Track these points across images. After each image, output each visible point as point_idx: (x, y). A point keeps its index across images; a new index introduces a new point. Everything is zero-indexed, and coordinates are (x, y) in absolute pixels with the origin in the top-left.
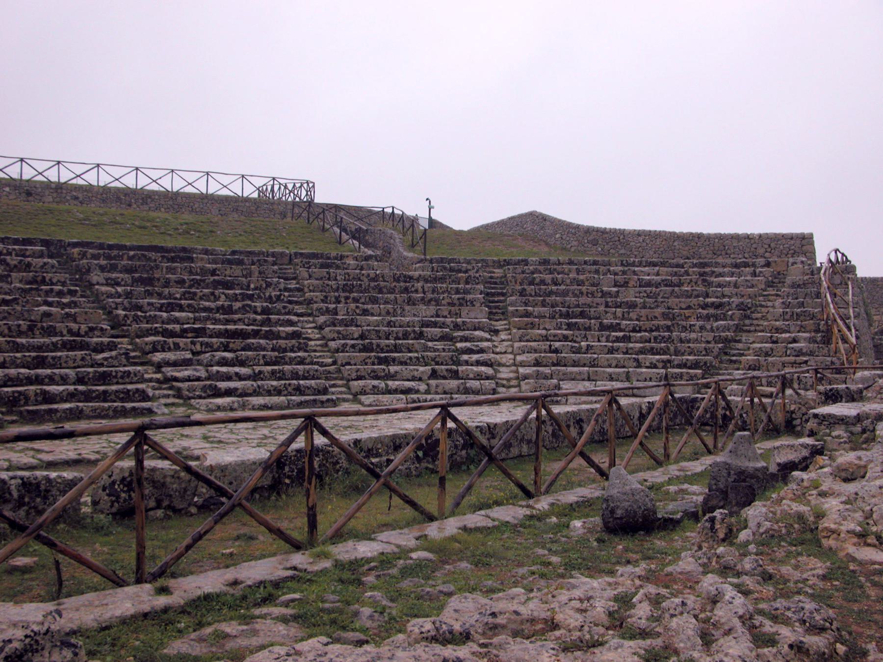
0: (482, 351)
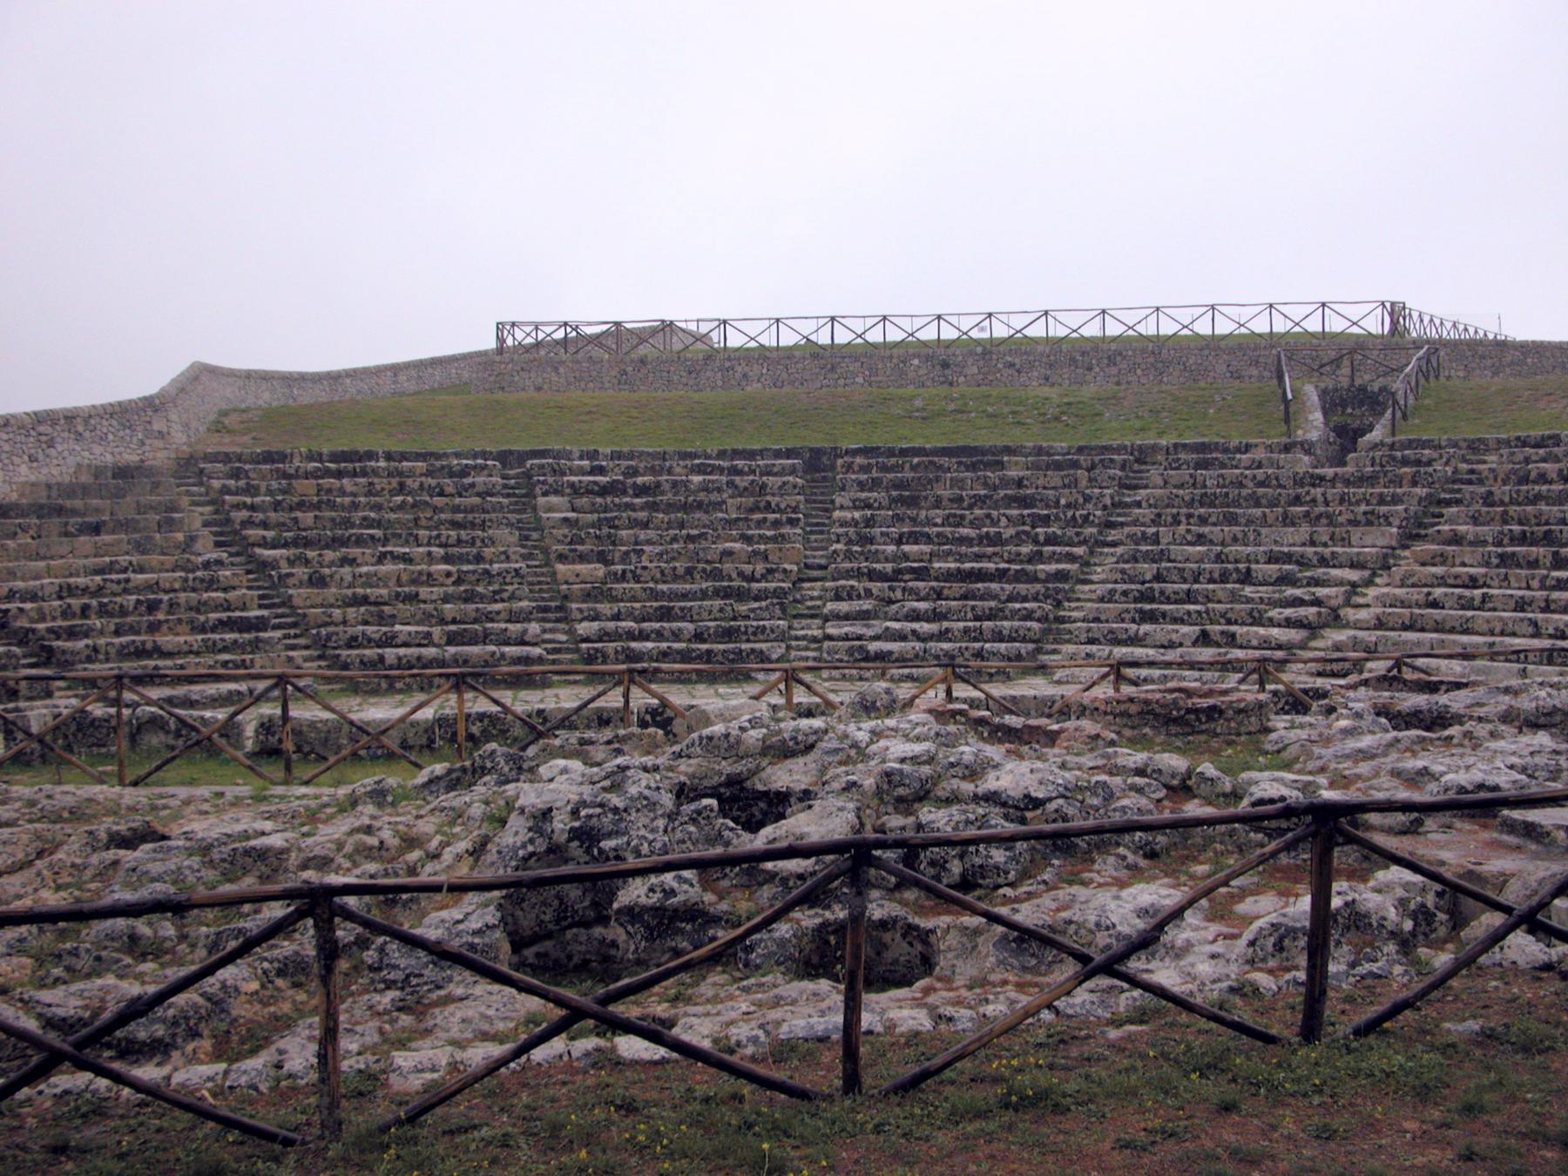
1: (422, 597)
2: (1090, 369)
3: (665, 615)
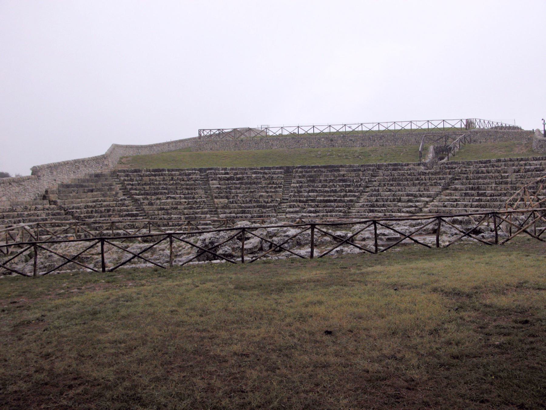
2: (374, 141)
3: (244, 212)
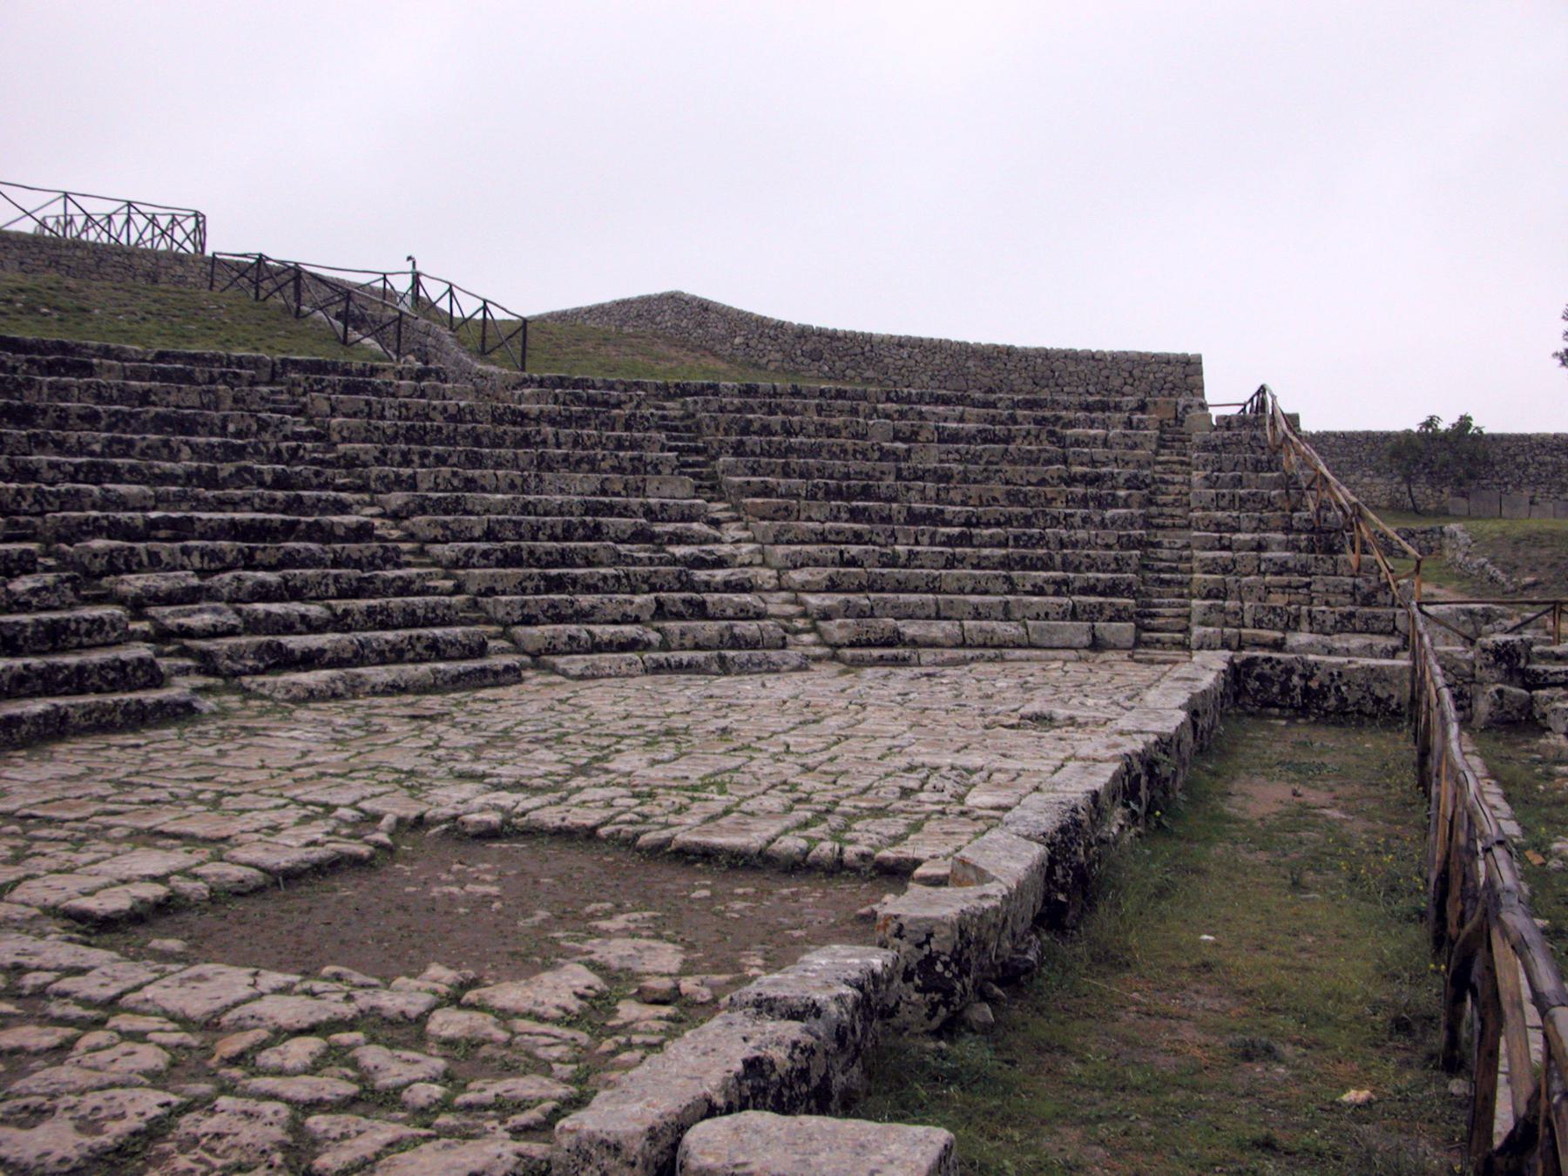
0: (720, 563)
1: (948, 517)
